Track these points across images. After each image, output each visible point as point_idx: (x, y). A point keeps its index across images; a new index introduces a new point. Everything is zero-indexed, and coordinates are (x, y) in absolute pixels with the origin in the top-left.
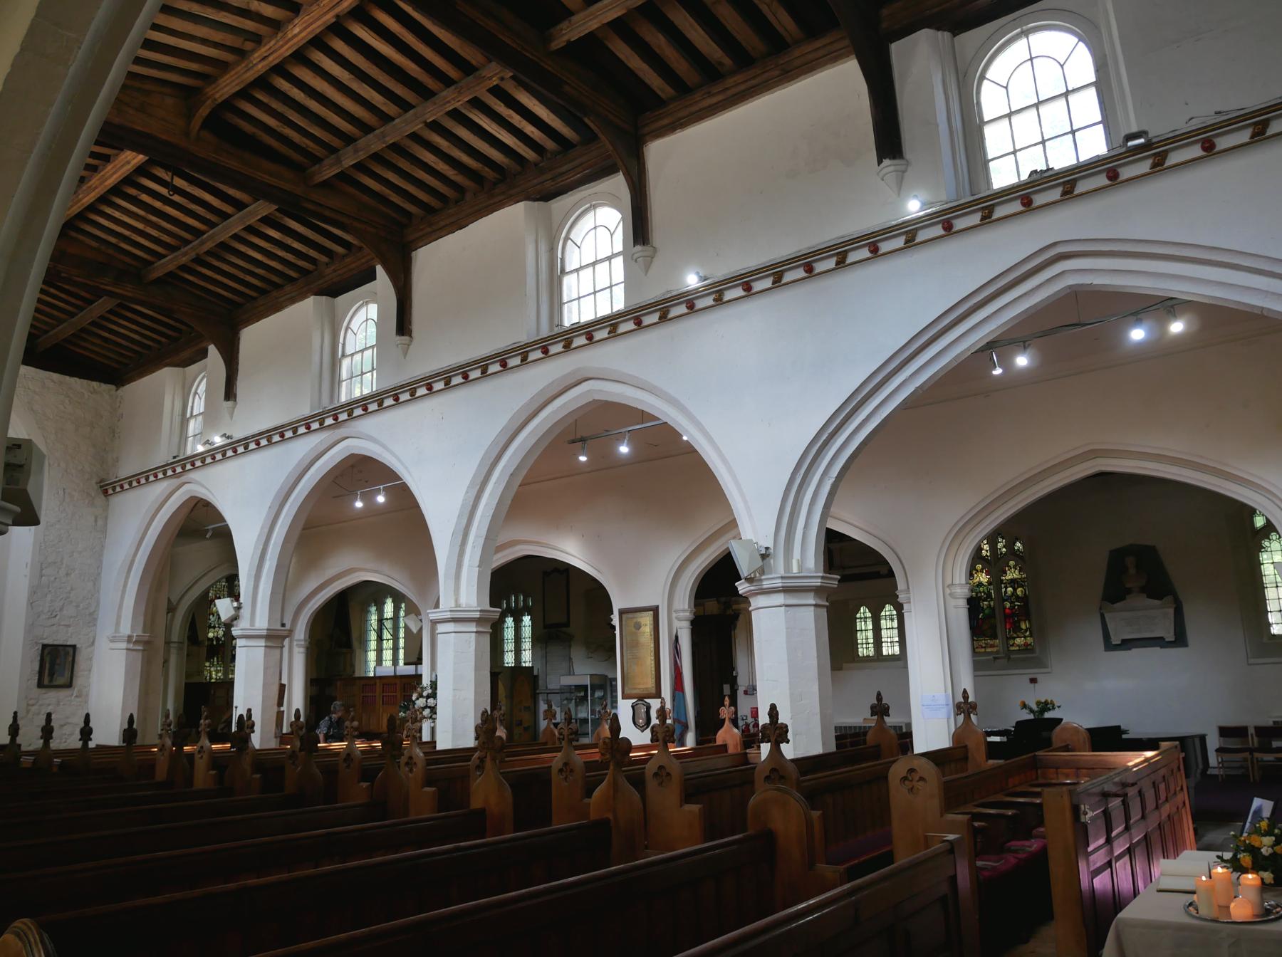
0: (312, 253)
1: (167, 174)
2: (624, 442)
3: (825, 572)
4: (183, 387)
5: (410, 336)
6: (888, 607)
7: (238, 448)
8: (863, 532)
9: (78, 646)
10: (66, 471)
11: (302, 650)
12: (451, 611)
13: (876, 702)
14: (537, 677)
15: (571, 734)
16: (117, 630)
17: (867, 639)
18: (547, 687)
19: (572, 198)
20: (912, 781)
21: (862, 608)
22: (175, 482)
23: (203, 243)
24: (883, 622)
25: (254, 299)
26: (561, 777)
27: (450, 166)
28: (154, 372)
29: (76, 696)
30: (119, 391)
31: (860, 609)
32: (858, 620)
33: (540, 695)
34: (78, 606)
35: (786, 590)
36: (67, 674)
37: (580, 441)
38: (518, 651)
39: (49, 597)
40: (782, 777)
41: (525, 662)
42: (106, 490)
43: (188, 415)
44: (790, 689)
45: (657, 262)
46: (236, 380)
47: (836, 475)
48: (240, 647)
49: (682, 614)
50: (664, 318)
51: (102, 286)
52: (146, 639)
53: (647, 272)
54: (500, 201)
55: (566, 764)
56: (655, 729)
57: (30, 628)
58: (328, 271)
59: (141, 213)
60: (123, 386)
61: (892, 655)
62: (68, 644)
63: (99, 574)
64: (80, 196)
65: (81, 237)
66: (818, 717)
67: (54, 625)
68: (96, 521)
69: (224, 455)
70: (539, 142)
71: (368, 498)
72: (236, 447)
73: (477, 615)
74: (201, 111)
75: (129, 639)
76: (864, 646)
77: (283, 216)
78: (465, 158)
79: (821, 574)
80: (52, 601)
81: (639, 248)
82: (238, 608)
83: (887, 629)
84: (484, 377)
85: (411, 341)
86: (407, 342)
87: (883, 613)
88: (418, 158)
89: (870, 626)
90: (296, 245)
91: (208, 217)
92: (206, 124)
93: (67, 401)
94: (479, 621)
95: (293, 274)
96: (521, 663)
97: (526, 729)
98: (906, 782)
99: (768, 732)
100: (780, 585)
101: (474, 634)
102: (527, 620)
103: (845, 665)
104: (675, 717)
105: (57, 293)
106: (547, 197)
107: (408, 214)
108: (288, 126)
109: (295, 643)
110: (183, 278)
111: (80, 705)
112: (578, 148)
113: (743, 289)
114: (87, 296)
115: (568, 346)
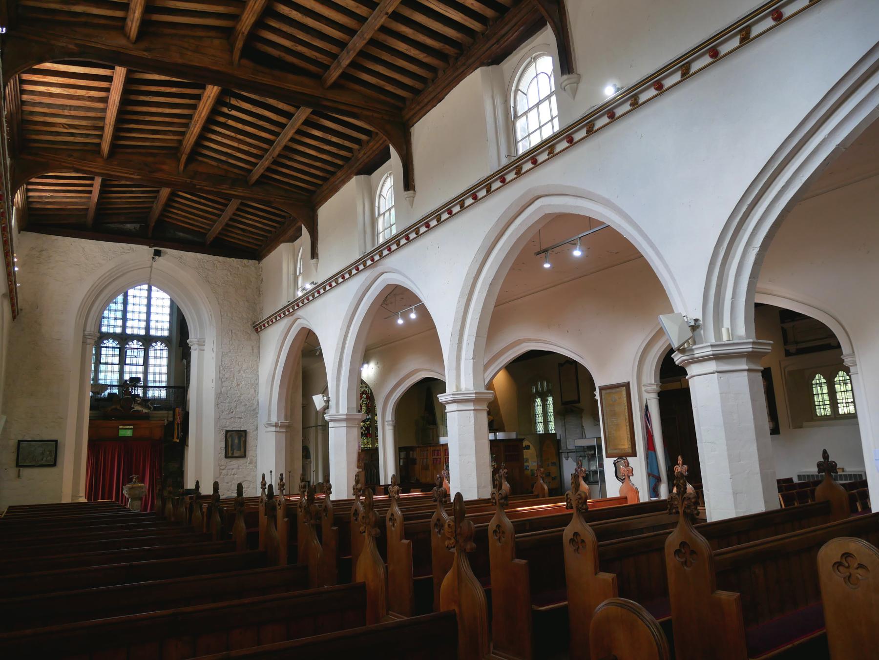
0: (347, 143)
1: (237, 101)
2: (576, 248)
3: (757, 337)
4: (294, 255)
5: (414, 190)
6: (841, 373)
7: (359, 267)
8: (815, 309)
9: (248, 431)
10: (232, 319)
11: (391, 428)
12: (453, 394)
13: (822, 460)
14: (559, 441)
15: (502, 499)
16: (269, 419)
17: (823, 401)
18: (567, 448)
19: (517, 56)
20: (848, 567)
21: (817, 376)
22: (291, 319)
23: (274, 148)
24: (837, 386)
25: (321, 185)
26: (496, 537)
27: (421, 51)
28: (276, 248)
29: (249, 463)
30: (261, 265)
31: (815, 377)
32: (814, 386)
33: (563, 453)
34: (245, 405)
35: (717, 357)
36: (242, 449)
37: (544, 252)
38: (546, 422)
39: (228, 400)
40: (693, 552)
41: (551, 430)
42: (257, 328)
43: (298, 274)
44: (728, 450)
45: (582, 86)
46: (317, 244)
47: (760, 245)
48: (331, 428)
49: (649, 388)
50: (591, 131)
51: (223, 191)
52: (287, 424)
53: (574, 98)
54: (463, 72)
55: (498, 526)
56: (569, 496)
57: (218, 420)
58: (360, 155)
59: (233, 134)
60: (262, 260)
61: (848, 414)
62: (242, 429)
63: (257, 384)
64: (192, 129)
65: (206, 160)
66: (758, 477)
67: (231, 418)
68: (253, 350)
69: (313, 296)
70: (479, 11)
71: (405, 316)
72: (321, 289)
73: (473, 396)
74: (237, 45)
75: (276, 425)
76: (822, 407)
77: (318, 118)
78: (429, 41)
79: (751, 340)
80: (230, 402)
81: (565, 77)
82: (328, 401)
83: (841, 392)
84: (463, 210)
85: (415, 194)
86: (412, 195)
87: (836, 379)
88: (393, 48)
89: (825, 390)
90: (334, 139)
91: (273, 129)
92: (245, 53)
93: (229, 274)
94: (474, 401)
95: (340, 162)
96: (548, 431)
97: (554, 479)
98: (841, 568)
99: (676, 503)
100: (711, 353)
101: (473, 411)
102: (550, 399)
103: (805, 424)
104: (650, 472)
105: (206, 202)
106: (497, 59)
107: (402, 99)
108: (299, 44)
109: (386, 423)
110: (274, 178)
111: (252, 469)
112: (511, 9)
113: (655, 88)
114: (223, 201)
115: (519, 173)
